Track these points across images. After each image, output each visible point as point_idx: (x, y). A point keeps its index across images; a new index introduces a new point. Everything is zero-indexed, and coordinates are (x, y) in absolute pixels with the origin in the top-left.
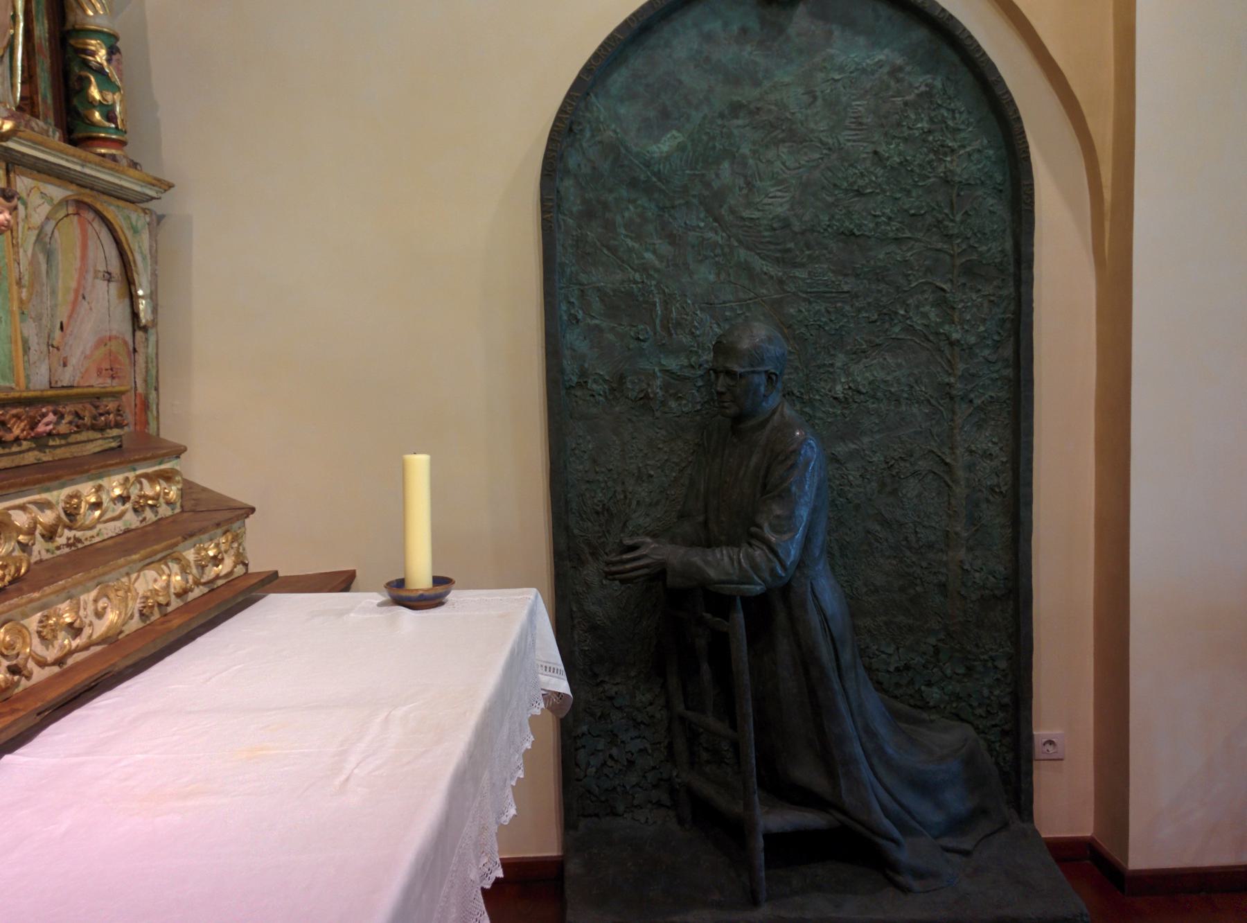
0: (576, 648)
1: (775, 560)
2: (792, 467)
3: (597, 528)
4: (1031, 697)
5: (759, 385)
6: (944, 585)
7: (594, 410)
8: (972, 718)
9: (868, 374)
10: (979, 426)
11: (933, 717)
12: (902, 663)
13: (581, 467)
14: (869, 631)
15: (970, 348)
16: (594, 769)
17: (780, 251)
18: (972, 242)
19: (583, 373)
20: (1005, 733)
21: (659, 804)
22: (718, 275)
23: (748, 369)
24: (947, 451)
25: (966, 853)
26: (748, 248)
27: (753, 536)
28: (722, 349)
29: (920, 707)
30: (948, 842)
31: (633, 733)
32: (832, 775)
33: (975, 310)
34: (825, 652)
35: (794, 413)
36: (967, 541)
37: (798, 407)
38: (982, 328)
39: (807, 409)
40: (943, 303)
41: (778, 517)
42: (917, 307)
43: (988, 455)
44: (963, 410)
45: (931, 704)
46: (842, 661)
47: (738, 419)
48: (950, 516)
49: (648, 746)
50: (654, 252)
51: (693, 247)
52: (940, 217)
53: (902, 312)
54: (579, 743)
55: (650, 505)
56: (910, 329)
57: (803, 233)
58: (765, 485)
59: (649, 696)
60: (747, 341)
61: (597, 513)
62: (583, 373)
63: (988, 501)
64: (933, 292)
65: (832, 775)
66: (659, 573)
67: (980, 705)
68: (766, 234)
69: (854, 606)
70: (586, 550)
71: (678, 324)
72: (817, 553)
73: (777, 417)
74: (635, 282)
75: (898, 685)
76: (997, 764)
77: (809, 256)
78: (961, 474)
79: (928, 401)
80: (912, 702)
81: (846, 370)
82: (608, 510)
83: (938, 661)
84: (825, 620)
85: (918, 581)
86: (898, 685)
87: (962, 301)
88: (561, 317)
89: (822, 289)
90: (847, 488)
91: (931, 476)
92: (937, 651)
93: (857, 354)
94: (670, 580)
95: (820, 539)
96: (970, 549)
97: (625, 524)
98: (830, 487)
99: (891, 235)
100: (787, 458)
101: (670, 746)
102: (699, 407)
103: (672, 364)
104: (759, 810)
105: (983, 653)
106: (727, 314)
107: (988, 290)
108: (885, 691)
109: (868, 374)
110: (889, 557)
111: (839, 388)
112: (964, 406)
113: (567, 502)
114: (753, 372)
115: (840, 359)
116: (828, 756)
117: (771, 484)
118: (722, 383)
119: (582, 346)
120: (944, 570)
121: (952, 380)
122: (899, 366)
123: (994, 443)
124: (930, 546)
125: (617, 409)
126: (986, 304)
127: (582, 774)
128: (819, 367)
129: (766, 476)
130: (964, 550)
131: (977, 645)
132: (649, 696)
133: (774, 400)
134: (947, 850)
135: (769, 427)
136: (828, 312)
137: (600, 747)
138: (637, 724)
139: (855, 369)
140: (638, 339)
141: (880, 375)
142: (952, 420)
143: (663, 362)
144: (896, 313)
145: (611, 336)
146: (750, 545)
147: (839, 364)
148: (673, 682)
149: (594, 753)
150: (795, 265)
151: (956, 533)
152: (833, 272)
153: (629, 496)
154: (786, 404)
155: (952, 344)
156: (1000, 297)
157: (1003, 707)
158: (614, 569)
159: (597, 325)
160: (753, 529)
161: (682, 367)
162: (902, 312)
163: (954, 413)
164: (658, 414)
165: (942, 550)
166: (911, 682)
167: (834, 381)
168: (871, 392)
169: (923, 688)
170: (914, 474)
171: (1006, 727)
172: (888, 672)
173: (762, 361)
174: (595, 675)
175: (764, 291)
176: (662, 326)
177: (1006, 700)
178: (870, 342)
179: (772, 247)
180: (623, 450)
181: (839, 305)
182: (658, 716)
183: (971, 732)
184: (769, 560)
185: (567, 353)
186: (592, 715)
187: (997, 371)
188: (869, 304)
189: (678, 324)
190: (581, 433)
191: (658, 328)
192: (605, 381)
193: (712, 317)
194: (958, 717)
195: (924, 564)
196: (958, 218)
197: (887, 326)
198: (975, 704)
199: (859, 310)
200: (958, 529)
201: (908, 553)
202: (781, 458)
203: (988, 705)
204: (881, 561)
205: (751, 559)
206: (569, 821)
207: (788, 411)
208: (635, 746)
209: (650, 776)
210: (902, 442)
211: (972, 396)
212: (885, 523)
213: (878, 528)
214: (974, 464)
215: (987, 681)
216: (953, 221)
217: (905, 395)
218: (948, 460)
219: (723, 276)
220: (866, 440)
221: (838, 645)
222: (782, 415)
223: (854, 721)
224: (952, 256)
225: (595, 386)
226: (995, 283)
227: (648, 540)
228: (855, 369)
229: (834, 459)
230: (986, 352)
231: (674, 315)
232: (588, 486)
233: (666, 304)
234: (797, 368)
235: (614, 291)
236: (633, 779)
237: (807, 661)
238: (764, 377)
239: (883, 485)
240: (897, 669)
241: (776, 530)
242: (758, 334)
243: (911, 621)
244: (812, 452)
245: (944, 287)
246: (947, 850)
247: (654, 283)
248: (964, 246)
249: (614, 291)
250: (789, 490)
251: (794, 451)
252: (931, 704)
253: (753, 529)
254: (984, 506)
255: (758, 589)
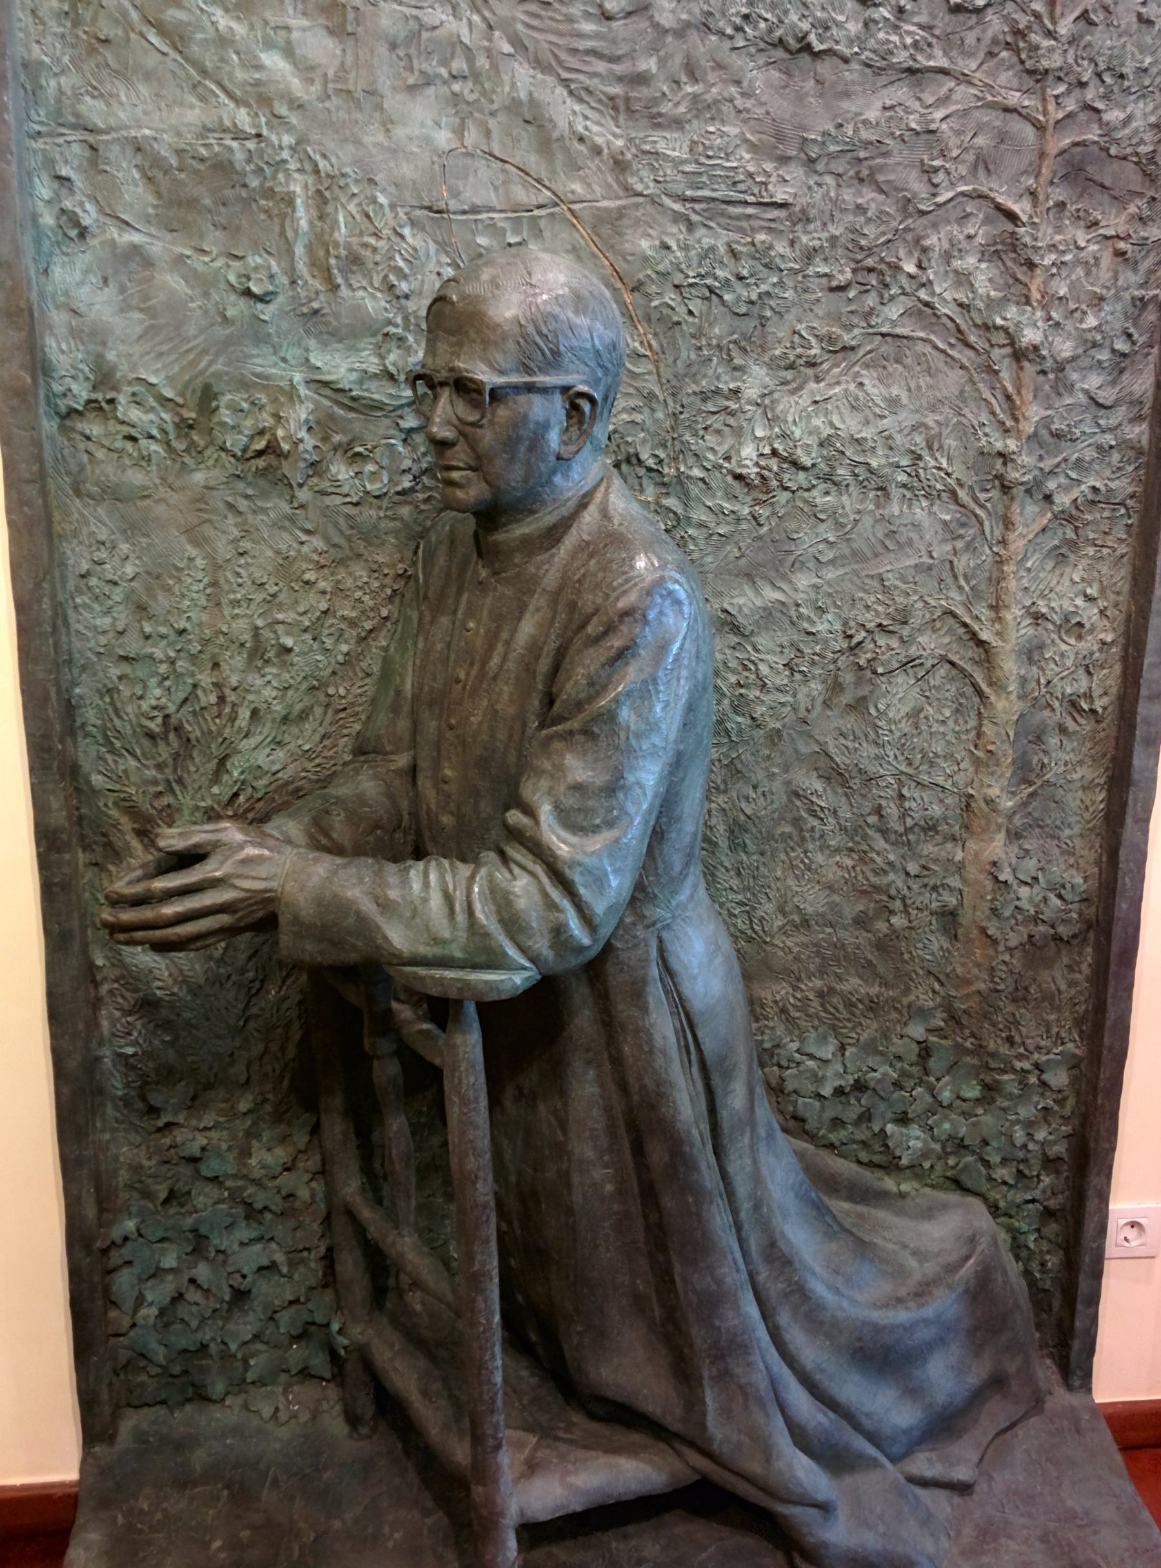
0: (106, 1051)
1: (566, 904)
2: (622, 655)
3: (151, 773)
4: (1113, 1149)
5: (546, 426)
6: (953, 914)
7: (136, 477)
8: (984, 1187)
9: (817, 422)
10: (1060, 559)
11: (904, 1187)
12: (850, 1080)
13: (105, 622)
14: (784, 1011)
15: (1060, 368)
16: (154, 1311)
17: (620, 79)
18: (1090, 95)
19: (104, 378)
20: (1048, 1214)
21: (306, 1374)
22: (459, 132)
23: (515, 379)
24: (985, 613)
25: (963, 1489)
26: (539, 64)
27: (516, 835)
28: (450, 318)
29: (879, 1166)
30: (924, 1464)
31: (244, 1232)
32: (684, 1372)
33: (1080, 271)
34: (686, 1106)
35: (635, 508)
36: (1010, 818)
37: (650, 493)
38: (1091, 321)
39: (671, 502)
40: (1010, 250)
41: (578, 788)
42: (947, 257)
43: (1075, 627)
44: (1029, 517)
45: (904, 1162)
46: (724, 1114)
47: (491, 515)
48: (977, 763)
49: (279, 1257)
50: (289, 51)
51: (393, 46)
52: (1023, 21)
53: (910, 268)
54: (116, 1257)
55: (285, 719)
56: (925, 312)
57: (680, 33)
58: (550, 700)
59: (281, 1154)
60: (516, 298)
61: (151, 735)
62: (104, 378)
63: (1063, 730)
64: (987, 221)
65: (684, 1372)
66: (261, 918)
67: (1004, 1161)
68: (588, 27)
69: (753, 962)
70: (126, 824)
71: (354, 261)
72: (677, 862)
73: (590, 516)
74: (239, 136)
75: (837, 1123)
76: (1027, 1273)
77: (695, 98)
78: (1010, 666)
79: (953, 493)
80: (864, 1156)
81: (765, 405)
82: (178, 729)
83: (927, 1072)
84: (688, 1021)
85: (898, 905)
86: (837, 1123)
87: (1053, 247)
88: (35, 217)
89: (723, 192)
90: (753, 693)
91: (943, 671)
92: (925, 1051)
93: (797, 368)
94: (285, 938)
95: (689, 825)
96: (1014, 836)
97: (222, 761)
98: (717, 688)
99: (901, 58)
100: (610, 629)
101: (329, 1260)
102: (406, 483)
103: (340, 366)
104: (507, 1461)
105: (1020, 1057)
106: (482, 241)
107: (1115, 222)
108: (811, 1137)
109: (817, 422)
110: (837, 850)
111: (748, 451)
112: (1031, 509)
113: (70, 709)
114: (530, 388)
115: (756, 380)
116: (682, 1333)
117: (561, 705)
118: (446, 411)
119: (100, 304)
120: (954, 882)
121: (1012, 444)
122: (893, 403)
123: (1089, 599)
124: (930, 828)
125: (199, 477)
126: (1107, 259)
127: (126, 1322)
128: (704, 396)
129: (556, 668)
130: (1001, 837)
131: (1010, 1040)
132: (281, 1154)
133: (588, 469)
134: (924, 1483)
135: (570, 541)
136: (734, 254)
137: (169, 1262)
138: (252, 1213)
139: (790, 406)
140: (248, 293)
141: (849, 424)
142: (1003, 542)
143: (316, 360)
144: (897, 268)
145: (174, 282)
146: (504, 858)
147: (751, 392)
148: (336, 1128)
149: (158, 1273)
150: (657, 122)
151: (989, 802)
152: (753, 147)
153: (232, 697)
154: (617, 482)
155: (1019, 355)
156: (1142, 244)
157: (1050, 1163)
158: (127, 916)
159: (135, 249)
160: (514, 817)
161: (365, 376)
162: (910, 268)
163: (1008, 524)
164: (303, 495)
165: (954, 839)
166: (866, 1117)
167: (738, 432)
168: (823, 467)
169: (890, 1128)
170: (908, 664)
171: (1053, 1204)
172: (819, 1096)
173: (554, 360)
174: (153, 1111)
175: (578, 187)
176: (313, 264)
177: (1059, 1149)
178: (831, 339)
179: (601, 67)
180: (214, 584)
181: (761, 237)
182: (304, 1194)
183: (983, 1220)
184: (552, 906)
185: (58, 318)
186: (147, 1195)
187: (1111, 430)
188: (833, 240)
189: (354, 261)
190: (103, 535)
191: (302, 267)
192: (164, 401)
193: (443, 246)
194: (958, 1185)
195: (913, 868)
196: (1064, 28)
197: (871, 300)
198: (995, 1159)
199: (810, 255)
200: (994, 792)
201: (880, 843)
202: (592, 627)
203: (1025, 1161)
204: (820, 858)
205: (502, 901)
206: (95, 1431)
207: (620, 502)
208: (256, 1256)
209: (284, 1318)
210: (886, 590)
211: (1051, 485)
212: (835, 775)
213: (818, 786)
214: (1041, 647)
215: (1026, 1111)
216: (1050, 34)
217: (902, 477)
218: (984, 636)
219: (472, 136)
220: (803, 580)
221: (716, 1081)
222: (605, 514)
223: (741, 1241)
224: (1040, 128)
225: (135, 414)
226: (1132, 209)
227: (231, 832)
228: (790, 406)
229: (729, 624)
230: (1094, 381)
231: (342, 233)
232: (126, 668)
233: (321, 200)
234: (651, 396)
235: (179, 152)
236: (244, 1327)
237: (640, 1123)
238: (558, 404)
239: (836, 687)
240: (839, 1092)
241: (571, 821)
242: (544, 284)
243: (874, 990)
244: (677, 623)
245: (1016, 208)
246: (924, 1483)
247: (287, 140)
248: (1071, 105)
249: (179, 152)
250: (609, 717)
251: (627, 613)
252: (904, 1162)
253: (514, 817)
254: (1053, 741)
255: (515, 979)
